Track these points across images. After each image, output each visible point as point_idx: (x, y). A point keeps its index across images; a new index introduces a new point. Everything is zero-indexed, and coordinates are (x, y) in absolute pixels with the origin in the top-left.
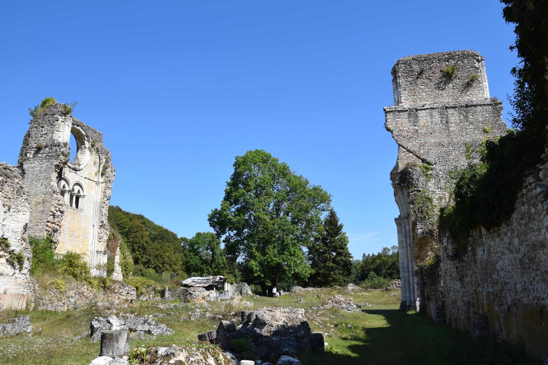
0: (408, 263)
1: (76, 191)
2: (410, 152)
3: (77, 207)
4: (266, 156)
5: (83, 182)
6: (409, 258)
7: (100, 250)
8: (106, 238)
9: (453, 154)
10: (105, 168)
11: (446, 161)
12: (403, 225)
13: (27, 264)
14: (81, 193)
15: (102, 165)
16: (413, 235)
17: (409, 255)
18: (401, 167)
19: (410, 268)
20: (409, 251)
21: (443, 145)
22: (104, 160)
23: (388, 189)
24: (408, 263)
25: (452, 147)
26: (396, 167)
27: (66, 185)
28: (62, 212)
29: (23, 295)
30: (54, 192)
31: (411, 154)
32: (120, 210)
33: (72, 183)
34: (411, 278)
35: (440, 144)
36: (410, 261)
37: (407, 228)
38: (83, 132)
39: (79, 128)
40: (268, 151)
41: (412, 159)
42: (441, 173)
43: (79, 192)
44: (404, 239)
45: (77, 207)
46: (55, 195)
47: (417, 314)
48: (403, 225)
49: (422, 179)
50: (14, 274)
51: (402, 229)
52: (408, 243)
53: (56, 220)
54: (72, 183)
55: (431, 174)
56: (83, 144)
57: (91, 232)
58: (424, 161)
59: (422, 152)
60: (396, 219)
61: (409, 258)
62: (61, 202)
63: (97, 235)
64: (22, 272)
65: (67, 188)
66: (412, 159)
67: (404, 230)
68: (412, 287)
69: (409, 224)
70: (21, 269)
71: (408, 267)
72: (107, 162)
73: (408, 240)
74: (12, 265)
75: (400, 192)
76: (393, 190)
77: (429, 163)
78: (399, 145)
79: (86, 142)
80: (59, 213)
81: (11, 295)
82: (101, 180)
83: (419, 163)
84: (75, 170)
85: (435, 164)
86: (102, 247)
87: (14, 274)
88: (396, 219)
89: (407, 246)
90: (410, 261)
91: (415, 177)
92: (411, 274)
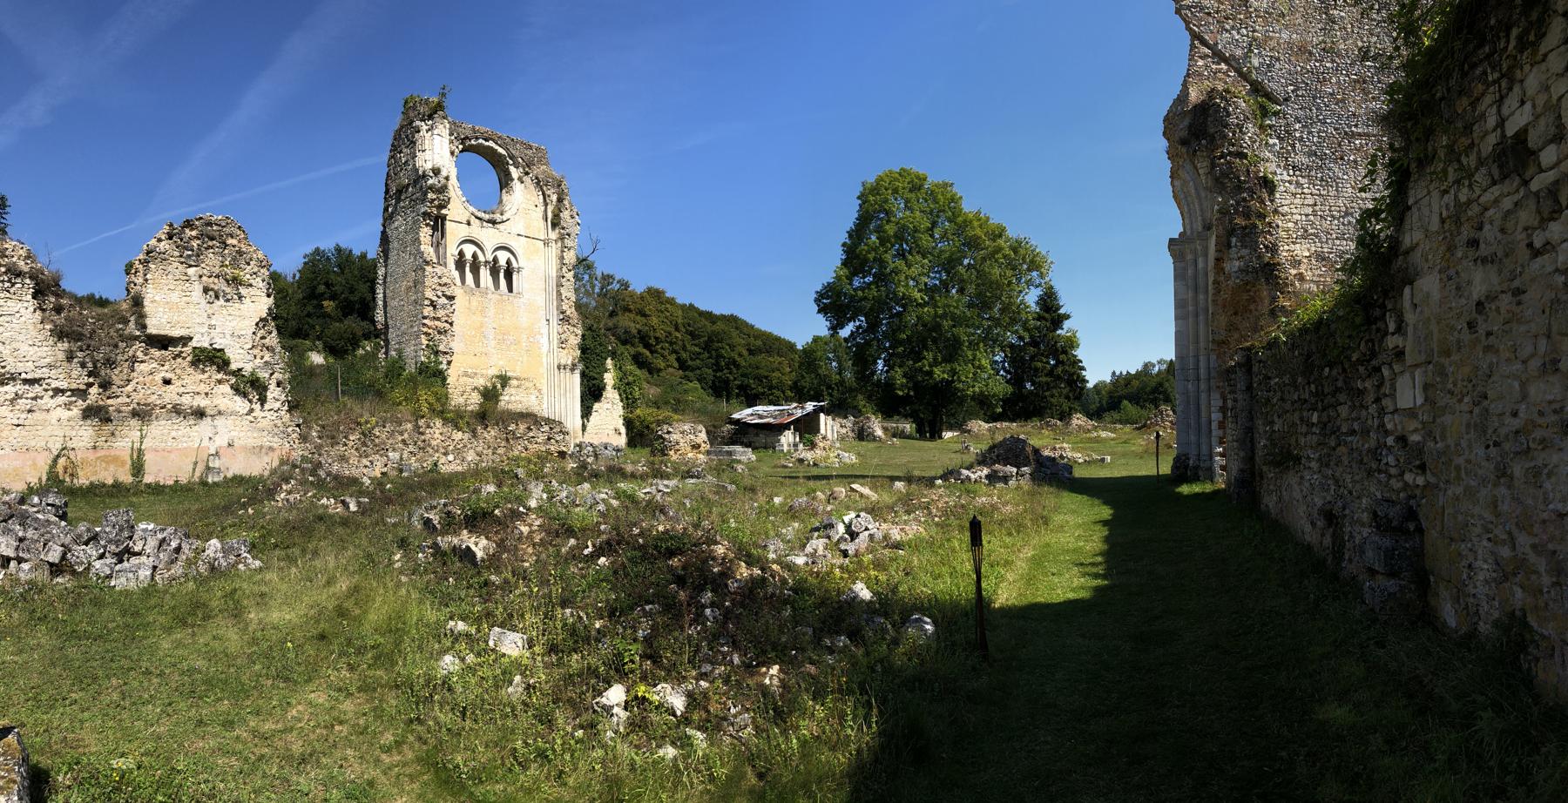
0: (1197, 357)
1: (502, 262)
2: (1219, 56)
3: (510, 289)
4: (918, 177)
5: (518, 245)
6: (1202, 345)
7: (563, 362)
8: (575, 340)
9: (1334, 80)
10: (556, 216)
11: (1315, 98)
12: (1190, 257)
13: (273, 392)
14: (515, 264)
15: (550, 209)
16: (1216, 282)
17: (1202, 339)
18: (1194, 95)
19: (1202, 371)
20: (1202, 326)
21: (1311, 53)
22: (554, 198)
23: (1151, 152)
24: (1197, 357)
25: (1333, 61)
26: (1183, 97)
27: (479, 253)
28: (451, 298)
29: (271, 449)
30: (427, 263)
31: (1223, 66)
32: (697, 310)
33: (489, 247)
34: (1203, 396)
35: (1303, 50)
36: (1202, 352)
37: (1201, 265)
38: (501, 150)
39: (491, 144)
40: (917, 168)
41: (1225, 79)
42: (1297, 126)
43: (508, 262)
44: (1191, 294)
45: (510, 289)
46: (429, 269)
47: (1216, 493)
48: (1190, 257)
49: (1251, 129)
50: (252, 410)
51: (1185, 269)
52: (1202, 304)
53: (440, 313)
54: (489, 247)
55: (1271, 127)
56: (508, 174)
57: (545, 330)
58: (1257, 89)
59: (1256, 62)
60: (1171, 240)
61: (1202, 345)
62: (444, 280)
63: (555, 337)
64: (267, 407)
65: (481, 258)
66: (1225, 79)
67: (1190, 272)
68: (1204, 420)
69: (1206, 255)
70: (263, 400)
71: (1197, 369)
72: (560, 200)
73: (1201, 297)
74: (245, 395)
75: (1189, 167)
76: (1169, 164)
77: (1269, 96)
78: (1196, 36)
79: (512, 169)
80: (443, 300)
81: (244, 448)
82: (553, 235)
83: (1243, 88)
84: (493, 222)
85: (1286, 100)
86: (570, 355)
87: (252, 410)
88: (1171, 240)
89: (1197, 315)
90: (1202, 352)
91: (1232, 120)
92: (1203, 386)
